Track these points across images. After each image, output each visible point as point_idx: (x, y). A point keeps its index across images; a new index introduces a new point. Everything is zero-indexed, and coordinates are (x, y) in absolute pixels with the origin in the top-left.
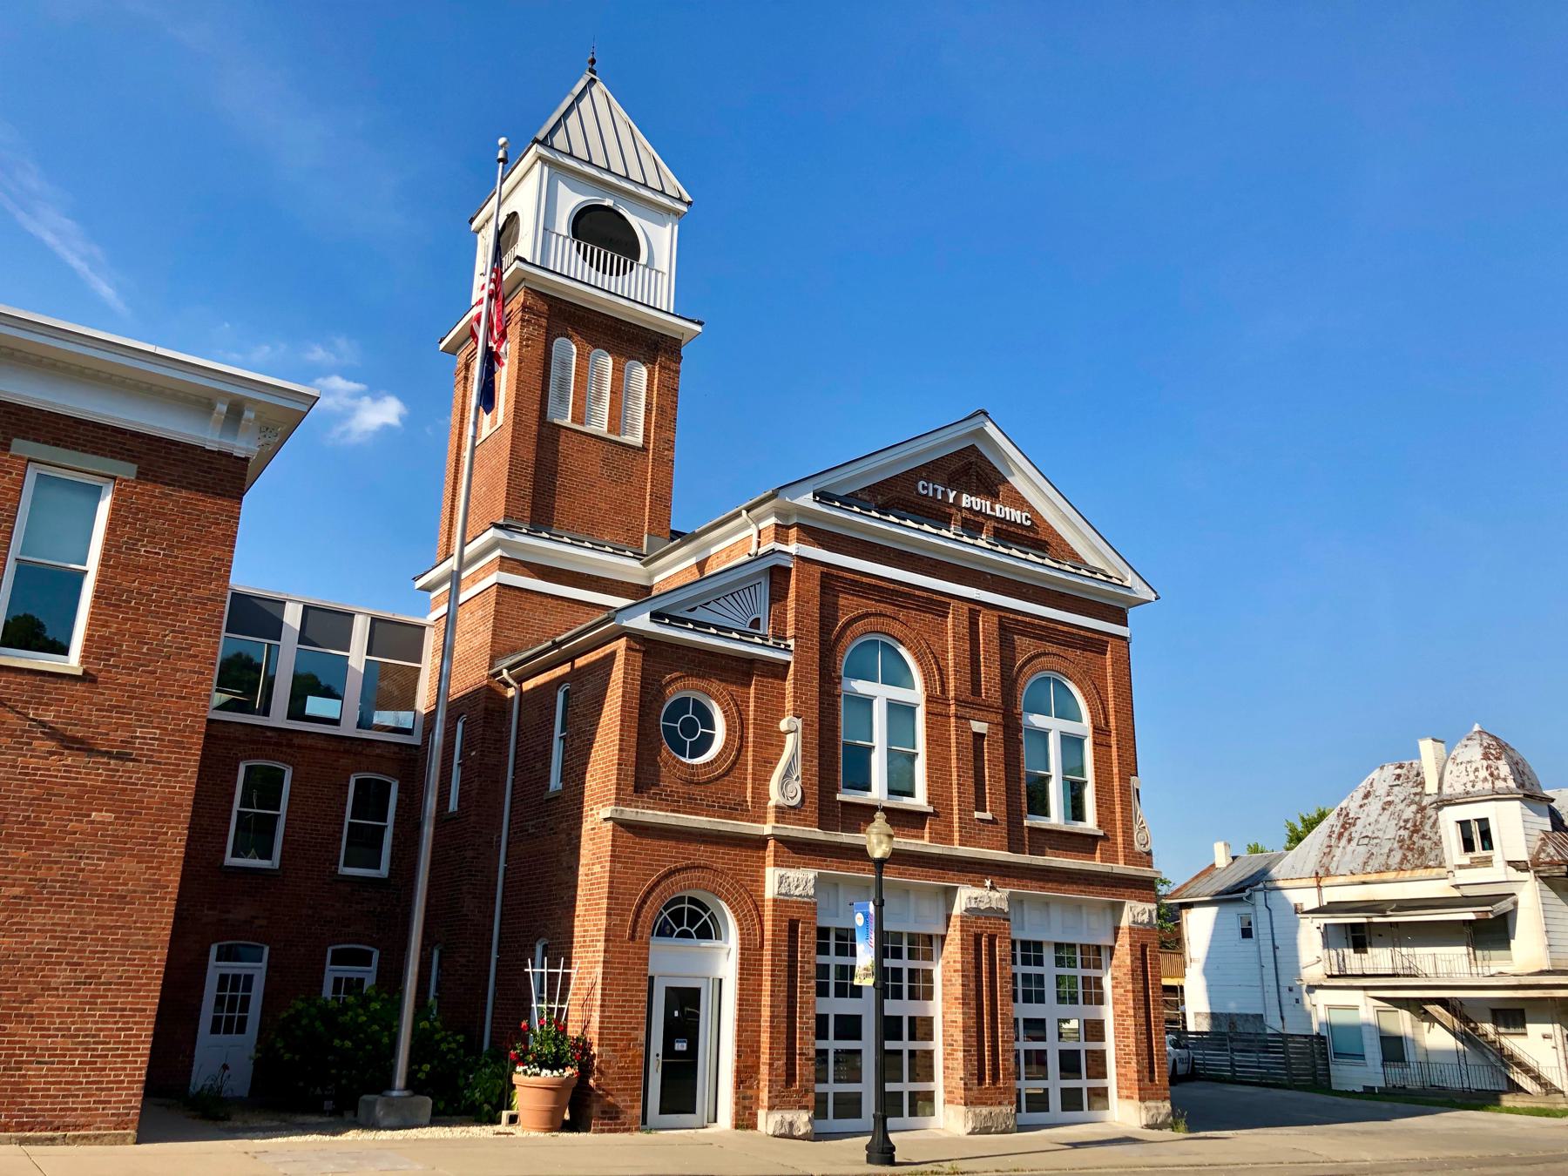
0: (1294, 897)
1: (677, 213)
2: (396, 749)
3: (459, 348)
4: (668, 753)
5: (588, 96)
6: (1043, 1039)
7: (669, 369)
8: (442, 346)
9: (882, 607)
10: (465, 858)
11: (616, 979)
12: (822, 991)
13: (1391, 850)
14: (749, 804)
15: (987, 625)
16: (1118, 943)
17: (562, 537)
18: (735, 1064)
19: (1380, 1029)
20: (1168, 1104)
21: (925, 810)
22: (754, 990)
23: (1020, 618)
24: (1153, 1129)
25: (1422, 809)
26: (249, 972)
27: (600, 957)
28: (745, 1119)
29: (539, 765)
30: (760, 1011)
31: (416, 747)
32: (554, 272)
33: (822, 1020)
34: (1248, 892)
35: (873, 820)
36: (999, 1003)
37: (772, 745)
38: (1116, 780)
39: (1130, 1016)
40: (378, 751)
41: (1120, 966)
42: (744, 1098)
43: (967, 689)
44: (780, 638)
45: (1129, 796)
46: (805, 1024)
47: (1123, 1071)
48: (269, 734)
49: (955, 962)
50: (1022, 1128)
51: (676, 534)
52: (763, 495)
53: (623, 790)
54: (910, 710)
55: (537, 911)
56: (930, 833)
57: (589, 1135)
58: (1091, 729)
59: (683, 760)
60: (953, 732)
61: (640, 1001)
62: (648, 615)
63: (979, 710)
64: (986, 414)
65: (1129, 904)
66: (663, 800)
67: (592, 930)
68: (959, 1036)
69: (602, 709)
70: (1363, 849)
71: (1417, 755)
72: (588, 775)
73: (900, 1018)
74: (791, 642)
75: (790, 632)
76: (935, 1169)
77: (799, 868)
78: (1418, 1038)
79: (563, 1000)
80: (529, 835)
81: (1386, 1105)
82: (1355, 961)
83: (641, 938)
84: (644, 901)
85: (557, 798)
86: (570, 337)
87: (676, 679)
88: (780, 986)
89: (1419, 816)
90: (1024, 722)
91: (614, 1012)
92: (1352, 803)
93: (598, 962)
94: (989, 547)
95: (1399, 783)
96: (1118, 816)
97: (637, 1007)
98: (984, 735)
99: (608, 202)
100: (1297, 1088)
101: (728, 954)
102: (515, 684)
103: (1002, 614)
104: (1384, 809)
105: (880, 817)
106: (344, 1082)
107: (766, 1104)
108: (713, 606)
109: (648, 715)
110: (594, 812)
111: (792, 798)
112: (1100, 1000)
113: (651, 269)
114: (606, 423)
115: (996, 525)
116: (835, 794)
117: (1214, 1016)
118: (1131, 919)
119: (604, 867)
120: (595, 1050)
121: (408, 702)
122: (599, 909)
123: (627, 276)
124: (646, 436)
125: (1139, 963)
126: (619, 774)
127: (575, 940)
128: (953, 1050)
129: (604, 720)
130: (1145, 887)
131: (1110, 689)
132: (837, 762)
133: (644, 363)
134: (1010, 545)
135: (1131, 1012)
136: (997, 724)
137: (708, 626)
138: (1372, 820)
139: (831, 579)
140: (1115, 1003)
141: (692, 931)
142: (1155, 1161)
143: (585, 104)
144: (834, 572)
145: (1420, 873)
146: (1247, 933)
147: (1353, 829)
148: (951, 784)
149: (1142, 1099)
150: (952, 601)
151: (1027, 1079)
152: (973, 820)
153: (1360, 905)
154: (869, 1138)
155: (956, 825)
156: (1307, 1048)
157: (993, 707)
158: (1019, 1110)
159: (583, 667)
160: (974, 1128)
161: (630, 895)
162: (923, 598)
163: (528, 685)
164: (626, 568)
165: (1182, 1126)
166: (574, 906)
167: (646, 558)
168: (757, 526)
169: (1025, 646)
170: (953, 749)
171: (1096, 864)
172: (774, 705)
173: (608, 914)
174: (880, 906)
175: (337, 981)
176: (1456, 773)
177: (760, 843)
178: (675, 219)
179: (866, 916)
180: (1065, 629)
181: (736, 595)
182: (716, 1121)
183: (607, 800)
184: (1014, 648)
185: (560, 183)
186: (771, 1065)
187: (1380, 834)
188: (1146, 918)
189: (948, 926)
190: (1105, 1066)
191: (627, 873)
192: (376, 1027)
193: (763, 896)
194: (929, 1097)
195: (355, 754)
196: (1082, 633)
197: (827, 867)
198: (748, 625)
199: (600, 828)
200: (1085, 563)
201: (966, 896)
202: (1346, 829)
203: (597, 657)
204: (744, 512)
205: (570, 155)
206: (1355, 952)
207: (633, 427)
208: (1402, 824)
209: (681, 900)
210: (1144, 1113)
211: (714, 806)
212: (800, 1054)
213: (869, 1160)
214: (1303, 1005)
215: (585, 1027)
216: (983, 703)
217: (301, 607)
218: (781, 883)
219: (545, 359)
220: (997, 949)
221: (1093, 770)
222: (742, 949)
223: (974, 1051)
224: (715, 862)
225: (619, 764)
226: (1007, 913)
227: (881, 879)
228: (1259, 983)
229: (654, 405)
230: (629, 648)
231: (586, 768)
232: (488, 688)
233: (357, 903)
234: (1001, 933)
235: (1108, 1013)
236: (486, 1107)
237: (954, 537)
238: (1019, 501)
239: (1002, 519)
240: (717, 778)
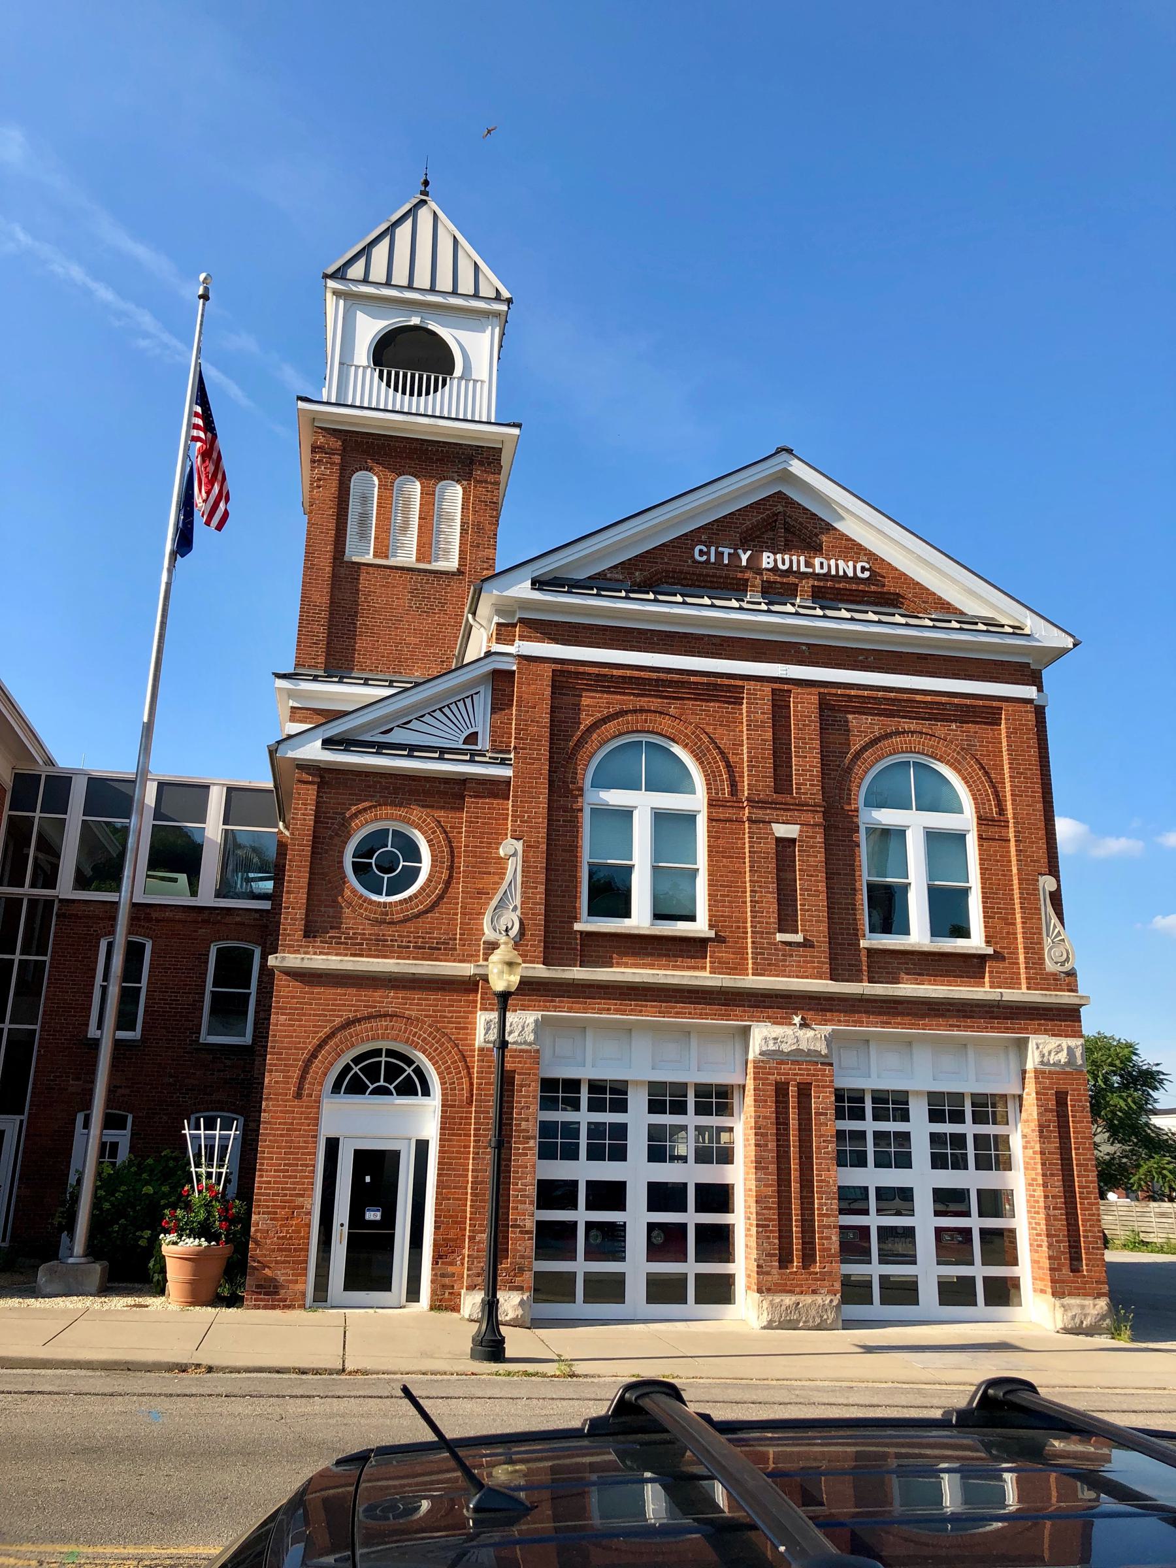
1: (497, 314)
2: (257, 916)
7: (486, 482)
9: (643, 702)
15: (803, 707)
16: (1026, 1090)
20: (1102, 1304)
21: (702, 935)
23: (853, 692)
24: (1078, 1334)
26: (114, 1140)
37: (489, 873)
40: (238, 919)
42: (443, 1275)
43: (768, 786)
46: (524, 1189)
54: (959, 838)
62: (319, 743)
63: (785, 810)
64: (790, 451)
65: (1034, 1040)
73: (575, 1183)
86: (370, 469)
87: (365, 810)
91: (274, 1177)
98: (793, 841)
99: (415, 321)
103: (822, 690)
108: (415, 725)
114: (415, 552)
115: (816, 583)
116: (572, 923)
118: (1038, 1059)
123: (439, 393)
136: (815, 825)
140: (1026, 1169)
141: (391, 1087)
144: (572, 668)
149: (1054, 1294)
150: (1004, 705)
152: (775, 944)
157: (808, 805)
160: (771, 1322)
161: (296, 1049)
162: (702, 684)
171: (983, 992)
180: (929, 698)
181: (446, 710)
184: (848, 731)
188: (1063, 1057)
195: (214, 923)
196: (956, 701)
198: (461, 741)
207: (447, 552)
210: (1059, 1313)
211: (408, 947)
213: (474, 1356)
221: (978, 871)
223: (773, 1226)
224: (408, 1009)
226: (826, 1056)
233: (219, 1071)
234: (816, 1081)
238: (852, 549)
239: (824, 575)
240: (417, 916)
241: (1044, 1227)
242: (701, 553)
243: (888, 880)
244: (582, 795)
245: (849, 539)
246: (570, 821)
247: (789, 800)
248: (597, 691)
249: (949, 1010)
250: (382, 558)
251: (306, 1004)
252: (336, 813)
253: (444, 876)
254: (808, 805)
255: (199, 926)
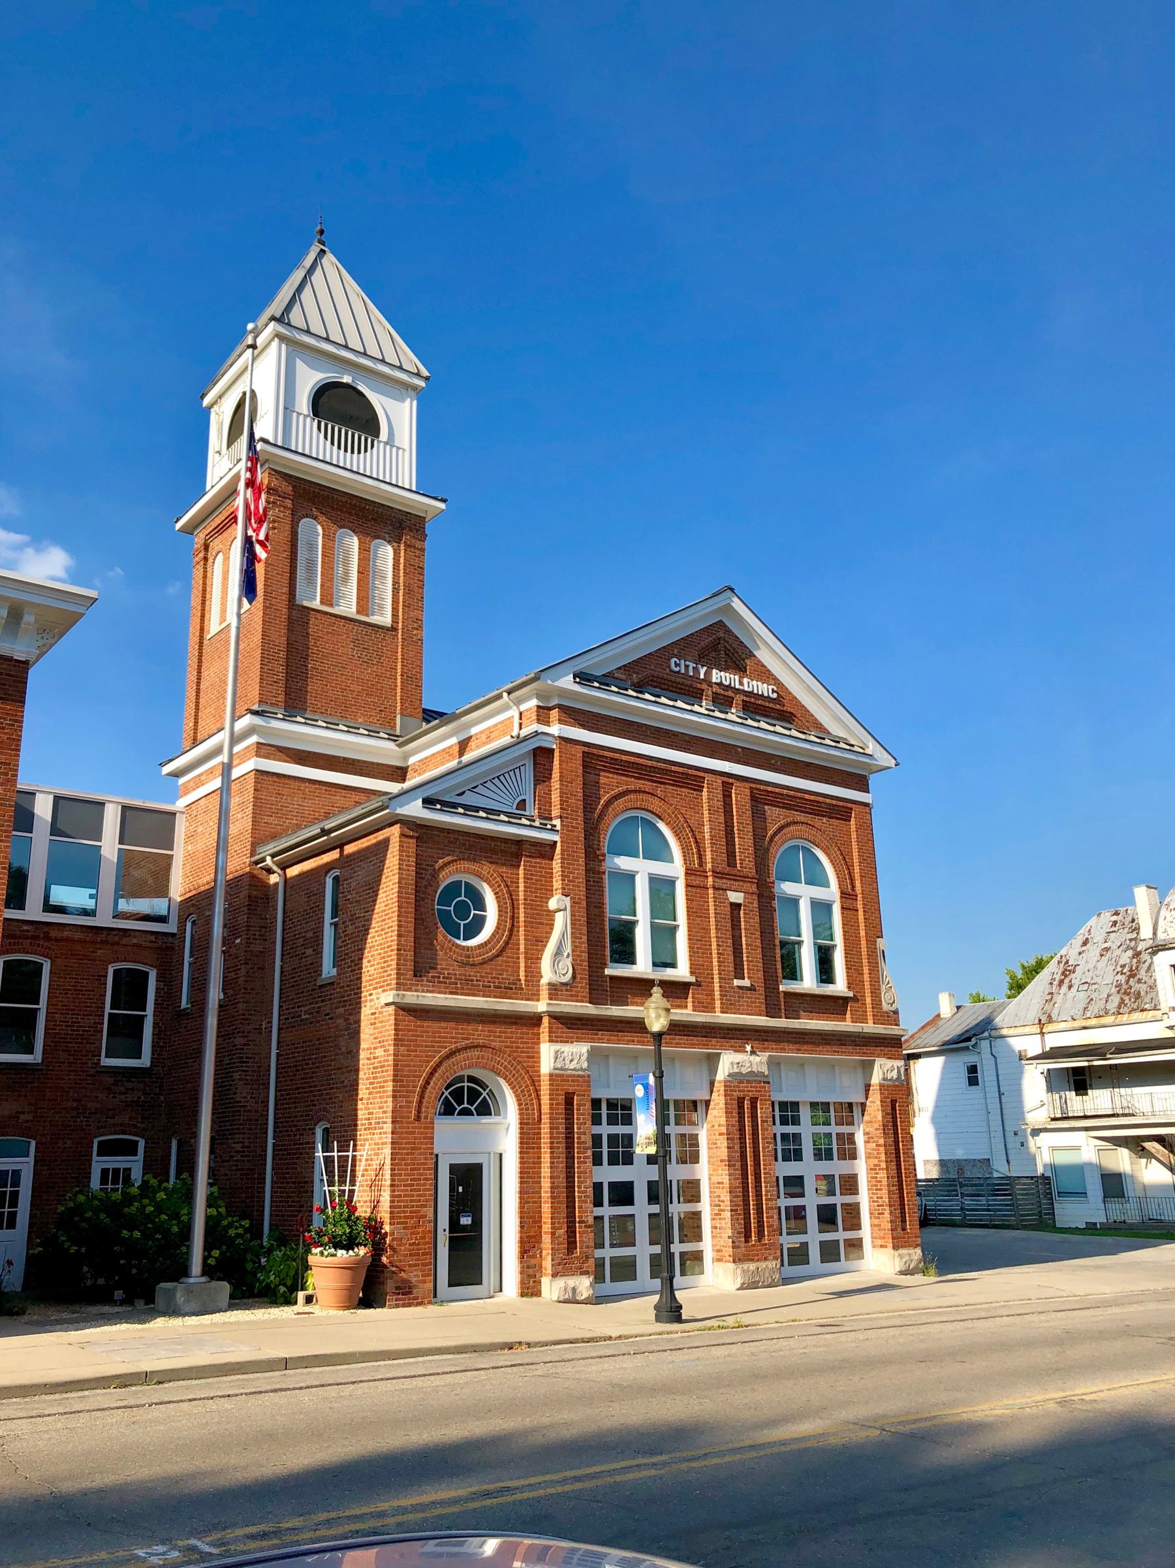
0: (1017, 1044)
1: (415, 388)
2: (153, 938)
3: (196, 527)
4: (444, 936)
5: (319, 268)
6: (802, 1195)
7: (414, 547)
8: (178, 526)
10: (235, 1045)
11: (404, 1159)
12: (597, 1161)
13: (1109, 996)
14: (523, 982)
15: (739, 797)
16: (870, 1099)
17: (317, 721)
18: (518, 1235)
19: (1100, 1167)
20: (919, 1251)
22: (534, 1163)
23: (770, 789)
25: (1137, 954)
27: (388, 1138)
28: (530, 1288)
29: (309, 951)
30: (540, 1182)
31: (173, 935)
32: (296, 452)
33: (598, 1187)
34: (974, 1040)
35: (651, 995)
36: (762, 1163)
37: (542, 924)
38: (863, 942)
39: (883, 1169)
40: (135, 941)
41: (871, 1122)
42: (528, 1267)
43: (723, 861)
44: (545, 818)
45: (876, 958)
46: (583, 1192)
47: (876, 1222)
48: (25, 928)
49: (719, 1125)
50: (786, 1281)
51: (429, 715)
52: (525, 678)
53: (403, 974)
54: (671, 882)
55: (314, 1096)
56: (693, 1002)
57: (385, 1310)
58: (838, 894)
59: (458, 942)
60: (711, 903)
61: (427, 1179)
62: (420, 801)
63: (735, 880)
64: (732, 590)
66: (441, 982)
67: (377, 1113)
68: (726, 1197)
69: (377, 895)
70: (1082, 995)
71: (1132, 901)
72: (365, 961)
74: (557, 822)
75: (555, 812)
76: (721, 1324)
77: (572, 1042)
78: (1137, 1174)
79: (353, 1183)
80: (302, 1020)
81: (1109, 1240)
82: (1076, 1103)
83: (426, 1118)
84: (427, 1083)
85: (331, 984)
87: (449, 863)
88: (559, 1158)
89: (1135, 960)
90: (776, 890)
91: (403, 1191)
92: (1071, 951)
93: (385, 1143)
94: (740, 721)
95: (1116, 929)
96: (866, 977)
97: (424, 1185)
98: (739, 905)
99: (347, 379)
100: (1025, 1228)
101: (507, 1129)
102: (279, 871)
103: (753, 786)
104: (1102, 955)
105: (657, 991)
106: (134, 1271)
107: (549, 1271)
109: (423, 899)
110: (374, 997)
111: (564, 975)
112: (853, 1156)
113: (392, 446)
115: (745, 698)
117: (943, 1163)
118: (881, 1077)
119: (388, 1050)
120: (387, 1228)
121: (161, 890)
122: (384, 1092)
123: (368, 453)
124: (395, 615)
125: (889, 1118)
126: (399, 959)
127: (359, 1122)
128: (719, 1210)
129: (379, 906)
130: (891, 1045)
131: (855, 854)
132: (604, 938)
133: (389, 542)
134: (758, 718)
135: (883, 1165)
137: (477, 809)
138: (1090, 966)
139: (593, 759)
141: (473, 1108)
142: (916, 1304)
143: (317, 277)
144: (595, 751)
145: (1137, 1016)
146: (973, 1081)
147: (1073, 976)
148: (711, 954)
149: (895, 1247)
151: (788, 1234)
152: (733, 988)
153: (1081, 1049)
154: (657, 1297)
155: (717, 994)
156: (1032, 1189)
157: (748, 877)
158: (782, 1265)
159: (354, 854)
160: (743, 1284)
162: (679, 773)
163: (293, 871)
164: (381, 749)
165: (932, 1271)
166: (357, 1090)
167: (401, 740)
168: (518, 708)
169: (775, 815)
170: (712, 920)
171: (846, 1025)
172: (543, 885)
173: (394, 1097)
174: (659, 1077)
175: (105, 1172)
176: (1169, 919)
177: (535, 1020)
178: (413, 394)
179: (646, 1087)
180: (812, 798)
181: (502, 778)
182: (501, 1291)
183: (388, 985)
185: (298, 361)
186: (553, 1234)
187: (1099, 980)
188: (894, 1074)
189: (712, 1092)
190: (859, 1218)
191: (410, 1056)
192: (164, 1217)
193: (539, 1071)
194: (698, 1257)
195: (113, 944)
196: (828, 801)
197: (600, 1040)
198: (515, 807)
199: (380, 1013)
200: (829, 733)
201: (729, 1062)
202: (1066, 976)
203: (369, 843)
204: (505, 695)
205: (308, 332)
206: (1077, 1095)
207: (381, 607)
208: (1119, 969)
209: (460, 1079)
210: (897, 1260)
212: (579, 1222)
213: (658, 1319)
214: (1028, 1148)
215: (375, 1207)
216: (738, 874)
217: (51, 798)
218: (556, 1058)
219: (291, 541)
220: (759, 1111)
221: (842, 933)
222: (521, 1123)
223: (740, 1210)
224: (494, 1041)
225: (398, 950)
226: (766, 1076)
227: (660, 1050)
228: (986, 1129)
229: (402, 584)
230: (402, 835)
231: (363, 954)
232: (252, 876)
233: (121, 1093)
235: (861, 1168)
236: (282, 1289)
237: (706, 712)
238: (765, 674)
240: (491, 959)
241: (887, 1200)
242: (677, 665)
243: (623, 917)
244: (604, 860)
245: (763, 666)
246: (598, 882)
247: (735, 872)
248: (609, 772)
249: (832, 1040)
250: (327, 605)
251: (418, 1036)
252: (428, 865)
253: (508, 925)
254: (748, 877)
255: (98, 945)
